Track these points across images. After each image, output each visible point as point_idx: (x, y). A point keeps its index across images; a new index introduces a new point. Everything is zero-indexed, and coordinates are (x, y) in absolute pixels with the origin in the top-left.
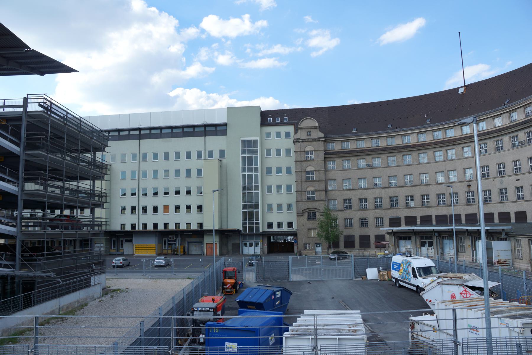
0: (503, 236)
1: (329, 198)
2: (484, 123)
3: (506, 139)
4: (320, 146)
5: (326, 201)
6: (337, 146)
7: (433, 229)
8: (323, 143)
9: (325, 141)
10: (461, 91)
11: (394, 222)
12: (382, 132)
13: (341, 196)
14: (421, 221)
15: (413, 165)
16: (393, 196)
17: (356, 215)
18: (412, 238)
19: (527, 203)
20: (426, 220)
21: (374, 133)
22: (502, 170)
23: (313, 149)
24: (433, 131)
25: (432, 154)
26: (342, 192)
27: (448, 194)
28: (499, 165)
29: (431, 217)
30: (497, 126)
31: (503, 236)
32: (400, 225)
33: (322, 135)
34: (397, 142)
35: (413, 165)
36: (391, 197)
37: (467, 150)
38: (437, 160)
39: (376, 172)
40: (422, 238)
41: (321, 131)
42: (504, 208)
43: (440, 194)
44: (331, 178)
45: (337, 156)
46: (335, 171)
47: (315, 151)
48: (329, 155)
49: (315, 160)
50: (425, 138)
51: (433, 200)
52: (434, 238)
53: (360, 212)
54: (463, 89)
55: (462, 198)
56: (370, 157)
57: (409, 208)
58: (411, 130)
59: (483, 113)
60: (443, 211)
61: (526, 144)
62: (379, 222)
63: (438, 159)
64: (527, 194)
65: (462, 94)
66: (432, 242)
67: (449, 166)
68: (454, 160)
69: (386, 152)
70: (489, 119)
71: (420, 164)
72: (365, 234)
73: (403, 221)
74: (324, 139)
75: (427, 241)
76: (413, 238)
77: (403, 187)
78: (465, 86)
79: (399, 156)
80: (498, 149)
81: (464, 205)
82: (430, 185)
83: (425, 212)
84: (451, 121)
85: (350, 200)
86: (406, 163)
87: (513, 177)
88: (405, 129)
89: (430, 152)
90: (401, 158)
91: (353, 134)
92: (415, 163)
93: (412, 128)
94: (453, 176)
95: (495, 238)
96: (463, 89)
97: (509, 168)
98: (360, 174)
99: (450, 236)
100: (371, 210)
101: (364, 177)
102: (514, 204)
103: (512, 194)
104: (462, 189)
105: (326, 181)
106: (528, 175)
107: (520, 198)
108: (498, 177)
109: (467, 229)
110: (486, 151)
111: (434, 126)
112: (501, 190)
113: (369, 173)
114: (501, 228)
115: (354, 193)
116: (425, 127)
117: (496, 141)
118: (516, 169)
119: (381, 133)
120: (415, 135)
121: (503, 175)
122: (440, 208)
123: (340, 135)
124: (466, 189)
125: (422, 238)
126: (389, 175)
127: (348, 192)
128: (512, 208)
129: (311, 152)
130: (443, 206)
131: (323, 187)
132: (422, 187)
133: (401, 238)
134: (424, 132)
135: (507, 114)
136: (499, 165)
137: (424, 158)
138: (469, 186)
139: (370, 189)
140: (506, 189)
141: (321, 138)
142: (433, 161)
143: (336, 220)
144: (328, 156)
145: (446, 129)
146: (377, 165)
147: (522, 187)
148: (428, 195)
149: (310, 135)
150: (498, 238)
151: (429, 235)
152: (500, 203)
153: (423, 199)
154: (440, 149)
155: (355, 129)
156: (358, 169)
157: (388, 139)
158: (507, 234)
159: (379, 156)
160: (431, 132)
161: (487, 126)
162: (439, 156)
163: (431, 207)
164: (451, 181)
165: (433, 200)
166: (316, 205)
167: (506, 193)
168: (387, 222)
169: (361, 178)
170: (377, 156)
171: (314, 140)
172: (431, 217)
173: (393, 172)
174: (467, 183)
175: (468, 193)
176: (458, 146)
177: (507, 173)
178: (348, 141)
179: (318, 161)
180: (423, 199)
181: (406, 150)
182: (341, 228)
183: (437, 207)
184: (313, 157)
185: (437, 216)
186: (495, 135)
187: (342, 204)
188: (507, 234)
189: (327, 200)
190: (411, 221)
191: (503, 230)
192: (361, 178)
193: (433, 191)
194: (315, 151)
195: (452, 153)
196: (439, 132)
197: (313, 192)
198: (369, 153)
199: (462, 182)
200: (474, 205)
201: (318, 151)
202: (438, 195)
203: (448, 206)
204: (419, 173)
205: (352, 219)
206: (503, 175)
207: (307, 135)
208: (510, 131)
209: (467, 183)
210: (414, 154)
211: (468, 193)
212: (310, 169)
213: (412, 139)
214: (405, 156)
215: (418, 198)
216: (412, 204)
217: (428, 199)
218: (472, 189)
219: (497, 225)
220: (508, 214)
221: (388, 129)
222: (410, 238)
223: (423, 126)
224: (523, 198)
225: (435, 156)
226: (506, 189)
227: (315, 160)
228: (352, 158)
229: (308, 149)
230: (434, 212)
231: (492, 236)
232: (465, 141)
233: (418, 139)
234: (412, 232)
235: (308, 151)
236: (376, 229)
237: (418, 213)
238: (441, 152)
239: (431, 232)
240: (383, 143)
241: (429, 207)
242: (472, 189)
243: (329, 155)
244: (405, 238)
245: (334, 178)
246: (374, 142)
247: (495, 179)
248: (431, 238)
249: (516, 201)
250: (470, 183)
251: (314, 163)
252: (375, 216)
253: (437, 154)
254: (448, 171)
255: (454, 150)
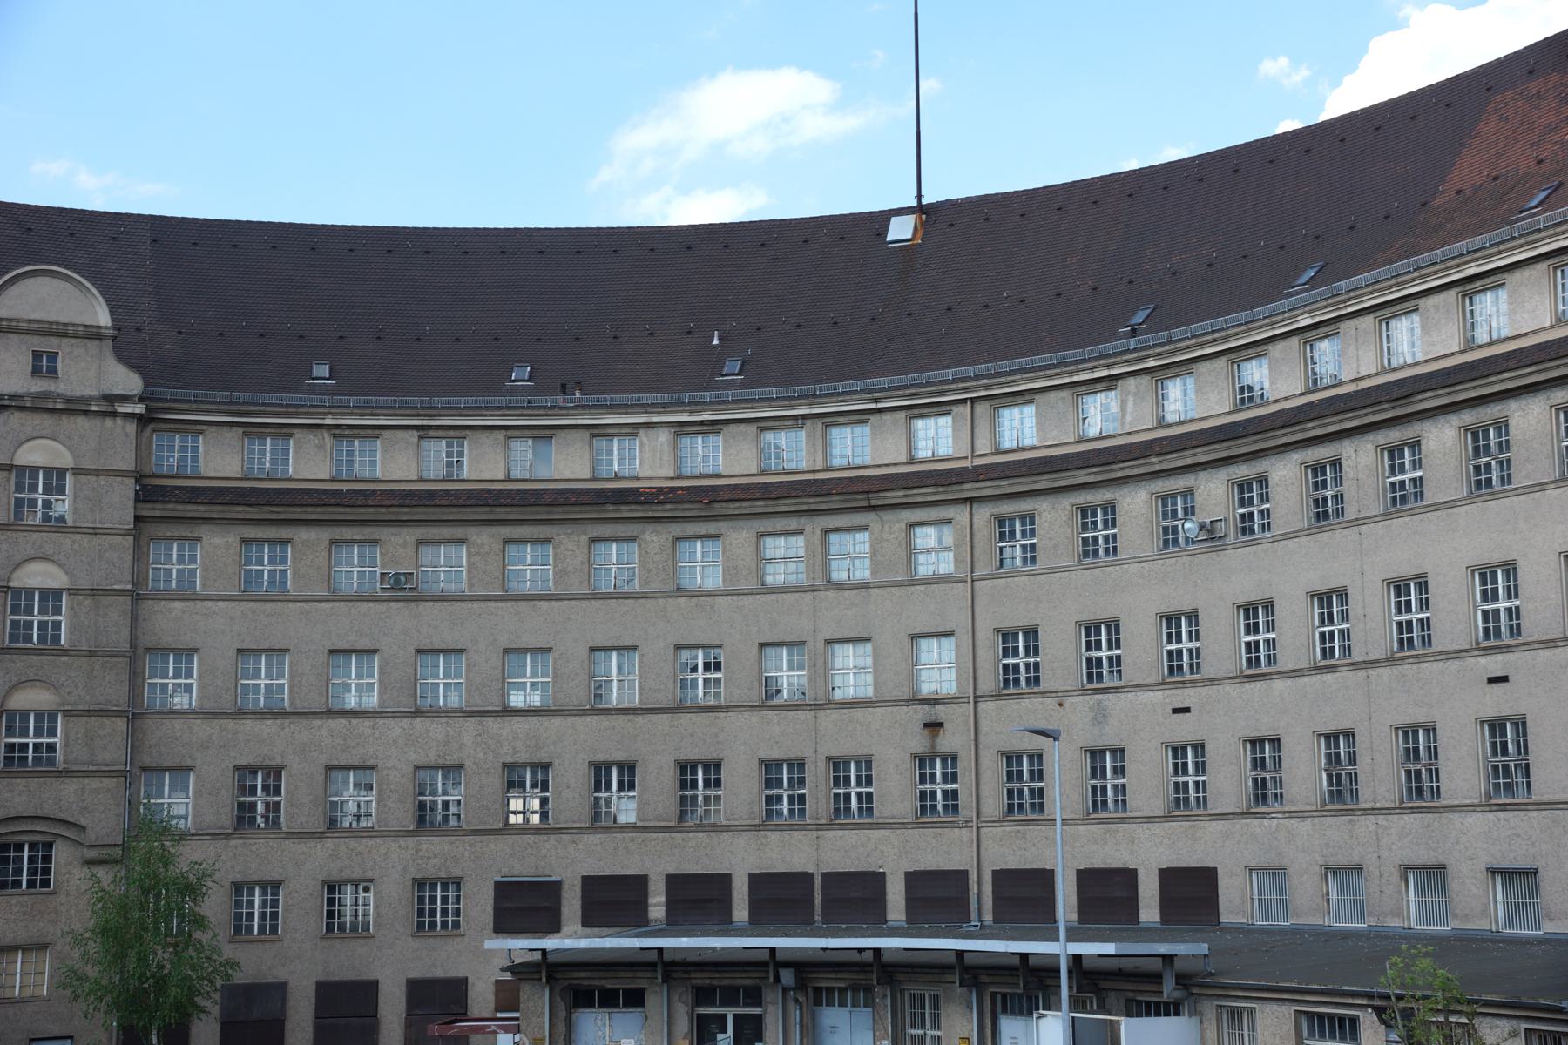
0: (1169, 990)
1: (147, 761)
2: (1029, 410)
3: (1135, 504)
4: (117, 444)
5: (123, 774)
6: (220, 459)
7: (773, 950)
8: (131, 428)
9: (143, 421)
10: (901, 229)
11: (526, 905)
12: (482, 401)
13: (218, 753)
14: (670, 904)
15: (645, 596)
16: (523, 757)
17: (302, 866)
18: (650, 999)
19: (1220, 825)
20: (699, 898)
21: (439, 401)
22: (1104, 654)
23: (66, 460)
24: (763, 424)
25: (750, 549)
26: (229, 724)
27: (822, 765)
28: (1091, 629)
29: (724, 880)
30: (1093, 432)
31: (1169, 990)
32: (554, 927)
33: (131, 382)
34: (567, 464)
35: (645, 596)
36: (509, 767)
37: (932, 542)
38: (769, 579)
39: (435, 624)
40: (703, 995)
41: (124, 357)
42: (1109, 849)
43: (778, 764)
44: (167, 640)
45: (215, 511)
46: (194, 598)
47: (78, 471)
48: (163, 505)
49: (76, 529)
50: (720, 457)
51: (741, 791)
52: (773, 998)
53: (329, 843)
54: (909, 221)
55: (895, 788)
56: (409, 535)
57: (607, 830)
58: (646, 408)
59: (1028, 361)
60: (792, 852)
61: (1231, 539)
62: (432, 902)
63: (775, 575)
64: (1548, 778)
65: (905, 250)
66: (758, 1020)
67: (836, 614)
68: (863, 586)
69: (501, 513)
70: (1053, 395)
71: (680, 592)
72: (350, 976)
73: (571, 904)
74: (139, 409)
75: (730, 1013)
76: (656, 1000)
77: (582, 712)
78: (920, 209)
79: (571, 542)
80: (1089, 549)
81: (904, 826)
82: (728, 708)
83: (941, 850)
84: (859, 384)
85: (275, 772)
86: (606, 585)
87: (1157, 696)
88: (608, 399)
89: (739, 537)
90: (581, 555)
91: (317, 399)
92: (655, 587)
93: (648, 398)
94: (853, 672)
95: (1112, 999)
96: (909, 221)
97: (1143, 648)
98: (344, 625)
99: (855, 989)
100: (1149, 819)
101: (364, 643)
102: (1157, 828)
103: (1147, 780)
104: (892, 747)
105: (138, 655)
106: (1232, 690)
107: (1185, 802)
108: (1083, 691)
109: (1024, 957)
110: (1030, 554)
111: (769, 401)
112: (1095, 754)
113: (399, 626)
114: (1163, 949)
115: (300, 731)
116: (718, 403)
117: (1164, 498)
118: (1174, 656)
119: (477, 410)
120: (664, 436)
121: (1107, 681)
122: (774, 836)
123: (242, 396)
124: (919, 743)
125: (703, 995)
126: (505, 641)
127: (268, 727)
128: (1148, 850)
129: (55, 476)
130: (792, 827)
131: (111, 687)
132: (685, 719)
133: (583, 998)
134: (714, 426)
135: (1145, 380)
136: (1091, 629)
137: (704, 564)
138: (934, 726)
139: (396, 714)
140: (1118, 752)
141: (124, 399)
142: (753, 584)
143: (191, 889)
144: (157, 510)
145: (831, 420)
146: (443, 584)
147: (1200, 748)
148: (713, 767)
149: (52, 372)
150: (1129, 1001)
151: (744, 980)
152: (1085, 820)
153: (687, 783)
154: (793, 524)
155: (321, 370)
156: (335, 597)
157: (516, 445)
158: (1184, 980)
159: (458, 532)
160: (752, 428)
161: (1041, 426)
162: (786, 559)
163: (727, 828)
164: (838, 695)
165: (741, 791)
166: (64, 797)
167: (1120, 771)
168: (479, 905)
169: (347, 652)
170: (446, 532)
171: (76, 407)
172: (722, 882)
173: (529, 626)
174: (923, 713)
175: (924, 760)
176: (888, 516)
177: (1286, 661)
178: (284, 432)
179: (94, 532)
180: (687, 783)
181: (611, 511)
182: (216, 936)
183: (758, 828)
184: (63, 507)
185: (756, 880)
186: (1083, 477)
187: (225, 795)
188: (1184, 980)
189: (139, 771)
190: (613, 900)
191: (1168, 959)
192: (347, 652)
193: (742, 745)
194: (78, 471)
195: (853, 552)
196: (793, 434)
197: (47, 719)
198: (405, 514)
199: (896, 702)
200: (953, 825)
201: (97, 473)
202: (770, 768)
203: (819, 827)
204: (674, 639)
205: (276, 886)
206: (1264, 669)
207: (36, 371)
208: (1157, 464)
209: (923, 713)
210: (655, 538)
211: (924, 760)
212: (37, 576)
213: (644, 458)
214: (685, 545)
215: (659, 777)
216: (626, 810)
217: (714, 782)
218: (949, 741)
219: (1149, 934)
220: (1128, 877)
221: (513, 392)
222: (635, 999)
223: (709, 396)
224: (1202, 802)
225: (762, 561)
226: (1118, 752)
227: (76, 529)
228: (303, 535)
229: (35, 454)
230: (741, 858)
231: (1098, 991)
232: (929, 494)
233: (678, 461)
234: (651, 966)
235: (34, 470)
236: (416, 944)
237: (657, 861)
238: (798, 543)
239: (862, 967)
240: (485, 463)
241: (716, 828)
242: (949, 741)
243: (163, 505)
244: (609, 1000)
245: (185, 641)
246: (436, 450)
247: (1069, 701)
248: (754, 996)
249: (1168, 817)
250: (941, 712)
251: (67, 541)
252: (414, 872)
253: (775, 547)
254: (828, 642)
255: (863, 537)
